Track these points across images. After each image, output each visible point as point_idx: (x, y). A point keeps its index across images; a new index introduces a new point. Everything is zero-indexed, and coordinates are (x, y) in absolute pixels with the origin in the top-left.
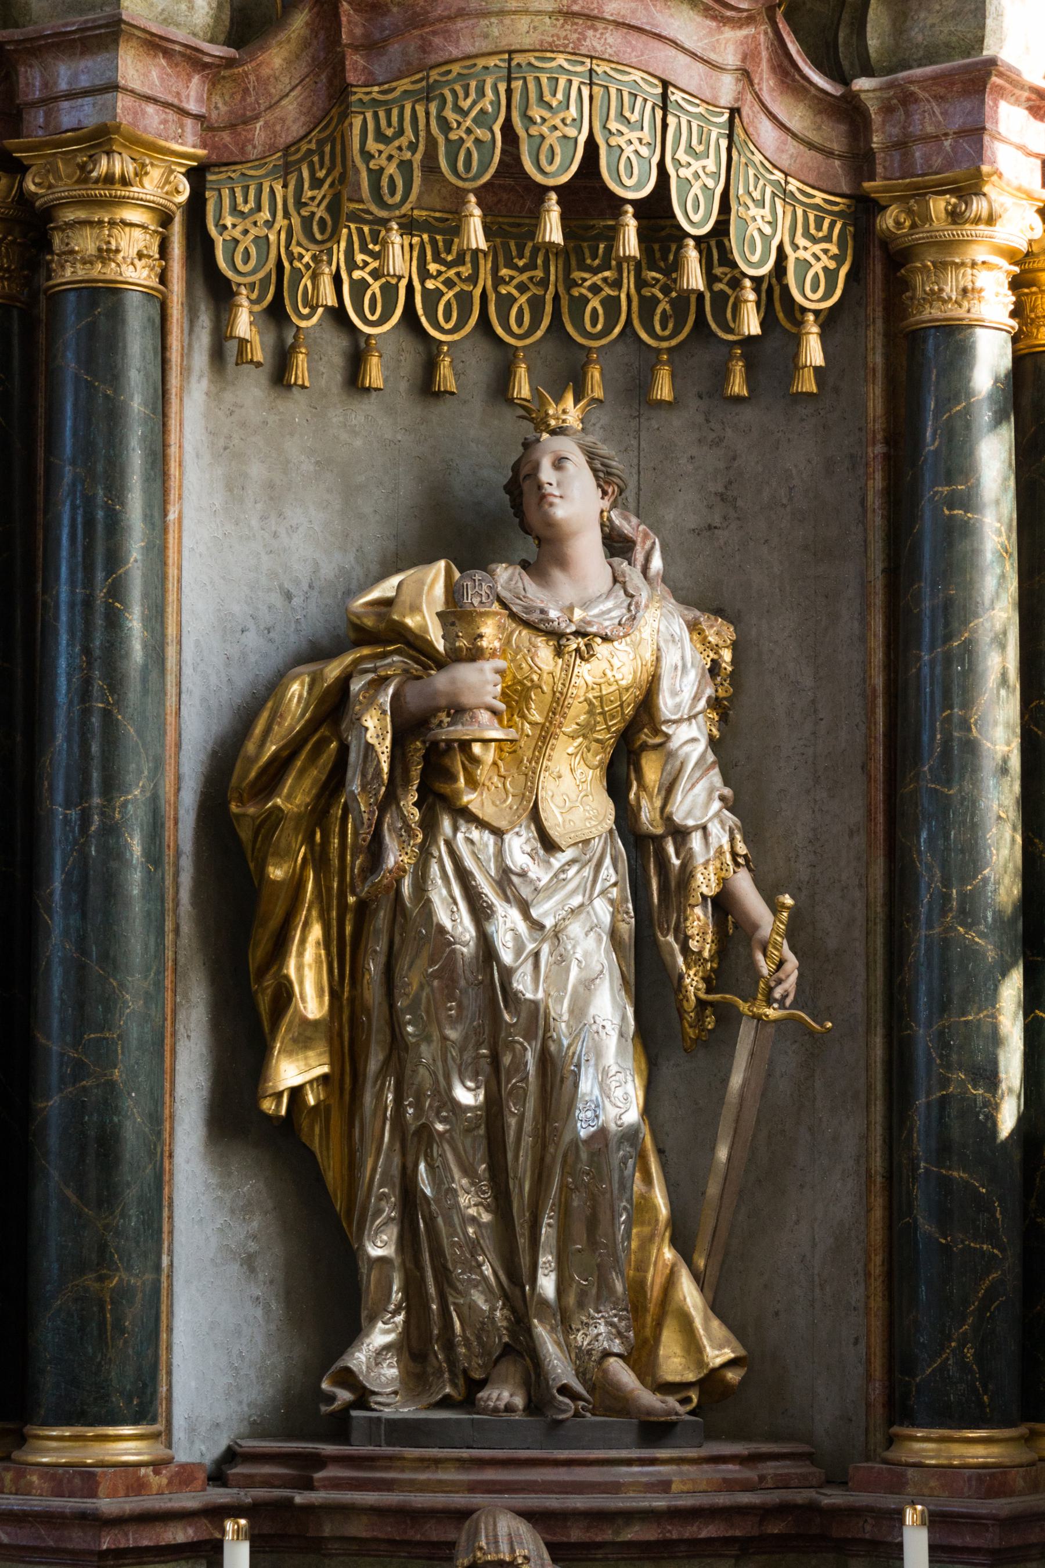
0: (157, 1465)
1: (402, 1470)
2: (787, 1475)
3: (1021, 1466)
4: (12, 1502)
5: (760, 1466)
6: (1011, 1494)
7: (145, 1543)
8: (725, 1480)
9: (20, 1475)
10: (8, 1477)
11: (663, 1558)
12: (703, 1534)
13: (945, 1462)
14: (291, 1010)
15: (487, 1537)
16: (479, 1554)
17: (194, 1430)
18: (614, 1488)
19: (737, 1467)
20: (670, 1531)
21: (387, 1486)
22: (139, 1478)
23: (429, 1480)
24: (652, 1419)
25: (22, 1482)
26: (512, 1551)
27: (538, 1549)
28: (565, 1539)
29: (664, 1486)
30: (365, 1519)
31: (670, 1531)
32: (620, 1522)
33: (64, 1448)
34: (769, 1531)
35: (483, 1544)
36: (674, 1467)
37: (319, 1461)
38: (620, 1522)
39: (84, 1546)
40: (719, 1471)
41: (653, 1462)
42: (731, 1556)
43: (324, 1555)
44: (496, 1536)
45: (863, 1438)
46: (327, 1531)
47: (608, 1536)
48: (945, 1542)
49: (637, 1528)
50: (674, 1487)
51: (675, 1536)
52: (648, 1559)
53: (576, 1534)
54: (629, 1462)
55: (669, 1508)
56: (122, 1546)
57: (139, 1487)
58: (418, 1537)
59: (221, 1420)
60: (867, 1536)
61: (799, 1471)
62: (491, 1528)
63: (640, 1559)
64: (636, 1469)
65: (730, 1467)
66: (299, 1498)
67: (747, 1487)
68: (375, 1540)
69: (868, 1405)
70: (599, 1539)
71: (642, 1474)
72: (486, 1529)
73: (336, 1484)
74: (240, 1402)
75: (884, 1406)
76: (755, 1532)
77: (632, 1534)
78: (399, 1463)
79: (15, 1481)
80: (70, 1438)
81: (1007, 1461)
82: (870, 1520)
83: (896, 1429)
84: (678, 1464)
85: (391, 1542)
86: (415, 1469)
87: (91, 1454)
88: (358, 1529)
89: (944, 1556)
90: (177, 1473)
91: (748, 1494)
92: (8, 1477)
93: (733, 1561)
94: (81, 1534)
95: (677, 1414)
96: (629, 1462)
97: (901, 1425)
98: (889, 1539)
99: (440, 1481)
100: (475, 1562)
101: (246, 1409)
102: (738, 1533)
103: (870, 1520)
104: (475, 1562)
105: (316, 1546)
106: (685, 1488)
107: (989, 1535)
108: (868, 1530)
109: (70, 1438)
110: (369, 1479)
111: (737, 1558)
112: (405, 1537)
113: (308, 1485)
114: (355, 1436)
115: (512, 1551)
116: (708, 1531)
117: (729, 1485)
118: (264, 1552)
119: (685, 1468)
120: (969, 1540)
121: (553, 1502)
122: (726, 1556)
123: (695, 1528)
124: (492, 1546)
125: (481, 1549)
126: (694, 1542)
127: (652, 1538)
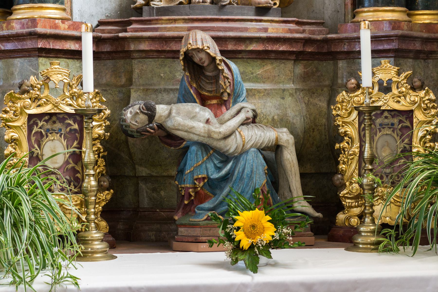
0: (63, 20)
1: (162, 24)
2: (313, 30)
3: (406, 21)
4: (5, 32)
5: (303, 27)
6: (403, 30)
7: (57, 47)
8: (289, 29)
9: (9, 24)
10: (4, 25)
11: (265, 59)
12: (281, 49)
13: (376, 19)
14: (197, 100)
15: (192, 39)
16: (189, 46)
17: (82, 16)
18: (246, 30)
19: (294, 25)
20: (267, 47)
21: (156, 30)
22: (55, 24)
23: (172, 27)
24: (260, 6)
25: (9, 27)
26: (203, 44)
27: (213, 45)
28: (226, 49)
29: (266, 30)
30: (147, 43)
31: (267, 47)
32: (248, 42)
33: (26, 12)
34: (307, 50)
35: (191, 42)
36: (269, 24)
37: (130, 23)
38: (248, 42)
39: (32, 47)
40: (287, 26)
41: (261, 21)
42: (292, 60)
43: (132, 59)
44: (196, 39)
45: (343, 18)
46: (132, 47)
47: (243, 48)
48: (376, 49)
49: (254, 45)
50: (269, 30)
51: (270, 49)
52: (260, 58)
53: (230, 47)
54: (251, 20)
55: (267, 37)
56: (47, 47)
57: (56, 27)
58: (168, 49)
59: (94, 14)
60: (345, 50)
61: (319, 29)
62: (194, 36)
63: (256, 58)
64: (254, 23)
65: (292, 25)
66: (121, 35)
67: (297, 32)
68: (151, 51)
69: (345, 5)
70: (239, 49)
71: (256, 25)
72: (192, 36)
73: (136, 30)
74: (102, 8)
75: (351, 5)
76: (301, 49)
77: (253, 47)
78: (160, 22)
79: (7, 27)
80: (28, 8)
81: (400, 19)
82: (346, 44)
83: (357, 10)
84: (271, 23)
85: (158, 51)
86: (167, 24)
87: (36, 14)
88: (144, 46)
89: (376, 56)
90: (72, 25)
91: (299, 34)
92: (4, 25)
93: (293, 62)
94: (30, 42)
95: (270, 3)
96: (251, 20)
97: (359, 8)
98: (354, 50)
99: (176, 27)
100: (188, 49)
101: (104, 11)
102: (295, 50)
103: (346, 44)
104: (188, 49)
105: (127, 55)
106: (274, 31)
107: (394, 44)
108: (346, 48)
109: (28, 8)
110: (149, 28)
111: (295, 61)
112: (163, 49)
113: (126, 31)
114: (144, 14)
115: (203, 44)
116: (283, 48)
117: (291, 31)
118: (109, 59)
119: (274, 24)
120: (386, 47)
121: (221, 34)
122: (290, 59)
123: (278, 46)
124: (194, 43)
125: (190, 44)
127: (260, 49)
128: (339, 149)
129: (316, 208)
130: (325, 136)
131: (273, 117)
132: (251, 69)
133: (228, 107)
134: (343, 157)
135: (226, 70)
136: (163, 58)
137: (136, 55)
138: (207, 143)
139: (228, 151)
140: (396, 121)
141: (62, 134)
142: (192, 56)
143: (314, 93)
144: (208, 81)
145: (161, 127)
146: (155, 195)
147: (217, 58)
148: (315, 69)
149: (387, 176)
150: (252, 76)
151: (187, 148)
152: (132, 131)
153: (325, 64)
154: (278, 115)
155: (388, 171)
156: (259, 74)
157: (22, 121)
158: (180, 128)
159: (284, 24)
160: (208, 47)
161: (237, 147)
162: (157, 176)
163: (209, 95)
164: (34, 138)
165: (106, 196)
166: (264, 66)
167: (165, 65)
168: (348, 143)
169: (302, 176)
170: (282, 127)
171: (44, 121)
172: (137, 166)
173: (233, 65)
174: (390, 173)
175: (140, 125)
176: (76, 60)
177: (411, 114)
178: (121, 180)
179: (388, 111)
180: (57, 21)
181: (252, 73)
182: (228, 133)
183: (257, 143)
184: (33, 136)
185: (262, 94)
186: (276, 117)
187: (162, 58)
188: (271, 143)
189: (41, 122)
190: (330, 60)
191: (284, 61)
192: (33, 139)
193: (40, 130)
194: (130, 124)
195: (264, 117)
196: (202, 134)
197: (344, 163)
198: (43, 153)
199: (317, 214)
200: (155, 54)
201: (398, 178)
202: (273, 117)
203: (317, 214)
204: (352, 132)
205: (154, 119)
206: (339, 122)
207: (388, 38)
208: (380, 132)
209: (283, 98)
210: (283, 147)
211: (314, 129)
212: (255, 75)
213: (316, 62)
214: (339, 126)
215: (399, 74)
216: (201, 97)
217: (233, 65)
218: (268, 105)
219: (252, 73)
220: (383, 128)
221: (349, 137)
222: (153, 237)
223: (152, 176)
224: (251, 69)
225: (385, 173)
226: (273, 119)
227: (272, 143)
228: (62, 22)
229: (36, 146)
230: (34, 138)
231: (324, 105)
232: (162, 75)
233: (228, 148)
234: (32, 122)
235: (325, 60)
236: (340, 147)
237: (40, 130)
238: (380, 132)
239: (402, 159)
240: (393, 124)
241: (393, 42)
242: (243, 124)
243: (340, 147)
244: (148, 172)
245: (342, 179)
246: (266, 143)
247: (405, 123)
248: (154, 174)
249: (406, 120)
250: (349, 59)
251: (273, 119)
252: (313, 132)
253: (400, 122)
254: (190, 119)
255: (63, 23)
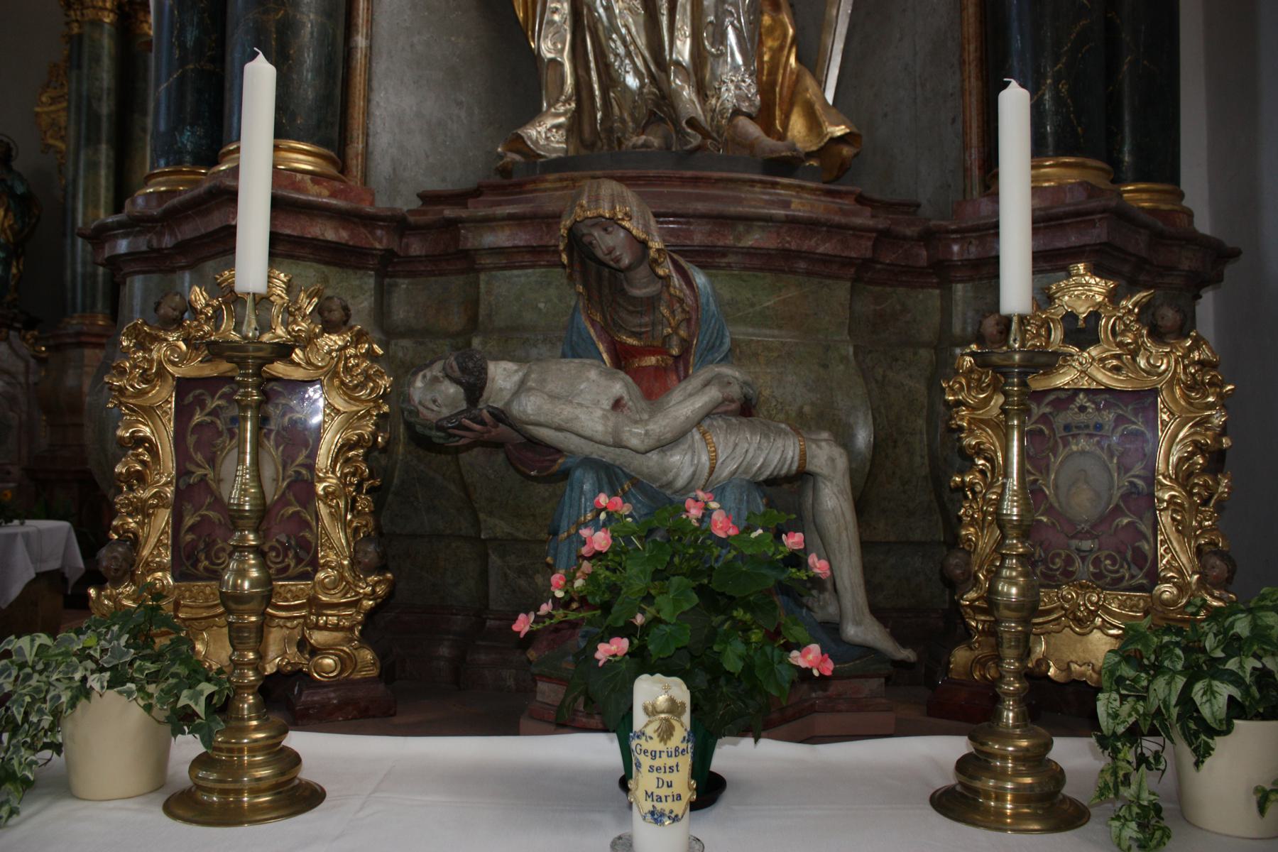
28: (688, 242)
54: (752, 183)
60: (972, 256)
63: (761, 270)
89: (1046, 266)
107: (1096, 232)
112: (541, 243)
123: (813, 243)
125: (582, 206)
126: (808, 256)
128: (961, 488)
129: (899, 637)
130: (922, 457)
131: (801, 408)
132: (750, 295)
133: (682, 374)
134: (971, 507)
135: (676, 280)
136: (544, 266)
137: (487, 261)
138: (617, 463)
139: (669, 484)
140: (1109, 417)
141: (270, 431)
142: (591, 243)
143: (897, 360)
144: (631, 308)
145: (500, 416)
146: (523, 582)
147: (651, 244)
148: (898, 307)
149: (1083, 559)
150: (751, 310)
151: (565, 474)
152: (424, 426)
153: (921, 296)
154: (813, 404)
155: (1087, 545)
156: (768, 307)
157: (164, 395)
158: (542, 419)
159: (829, 199)
160: (626, 214)
161: (694, 474)
162: (526, 540)
163: (635, 343)
164: (195, 437)
165: (370, 588)
166: (780, 289)
167: (549, 284)
168: (983, 472)
169: (866, 546)
170: (820, 428)
171: (220, 398)
172: (482, 516)
173: (700, 279)
174: (1091, 550)
175: (446, 412)
176: (350, 272)
177: (1150, 400)
178: (454, 545)
179: (1087, 391)
180: (299, 176)
181: (753, 305)
182: (669, 435)
183: (750, 465)
184: (192, 433)
185: (775, 354)
186: (807, 409)
187: (541, 266)
188: (786, 466)
189: (213, 397)
190: (933, 286)
191: (828, 282)
192: (191, 440)
193: (208, 419)
194: (420, 408)
195: (779, 407)
196: (599, 437)
197: (973, 523)
198: (222, 476)
199: (907, 654)
200: (527, 257)
201: (1114, 564)
202: (801, 408)
203: (907, 654)
204: (993, 444)
205: (481, 395)
206: (962, 419)
207: (1080, 217)
208: (1065, 446)
209: (825, 366)
210: (820, 479)
211: (895, 442)
212: (758, 308)
213: (901, 290)
214: (961, 429)
215: (1113, 297)
216: (615, 349)
217: (700, 279)
218: (790, 378)
219: (753, 305)
220: (1074, 436)
221: (986, 459)
222: (511, 683)
223: (516, 540)
224: (750, 295)
225: (1079, 550)
226: (800, 413)
227: (791, 465)
228: (312, 180)
229: (199, 457)
230: (195, 437)
231: (920, 387)
232: (541, 306)
233: (670, 476)
234: (190, 398)
235: (922, 287)
236: (963, 481)
237: (208, 419)
238: (1065, 446)
239: (1126, 516)
240: (1099, 427)
241: (1094, 227)
242: (708, 415)
243: (963, 481)
244: (508, 529)
245: (968, 563)
246: (772, 467)
247: (1134, 423)
248: (521, 535)
249: (1136, 415)
250: (980, 279)
251: (800, 413)
252: (895, 447)
253: (1120, 420)
254: (575, 401)
255: (314, 182)
